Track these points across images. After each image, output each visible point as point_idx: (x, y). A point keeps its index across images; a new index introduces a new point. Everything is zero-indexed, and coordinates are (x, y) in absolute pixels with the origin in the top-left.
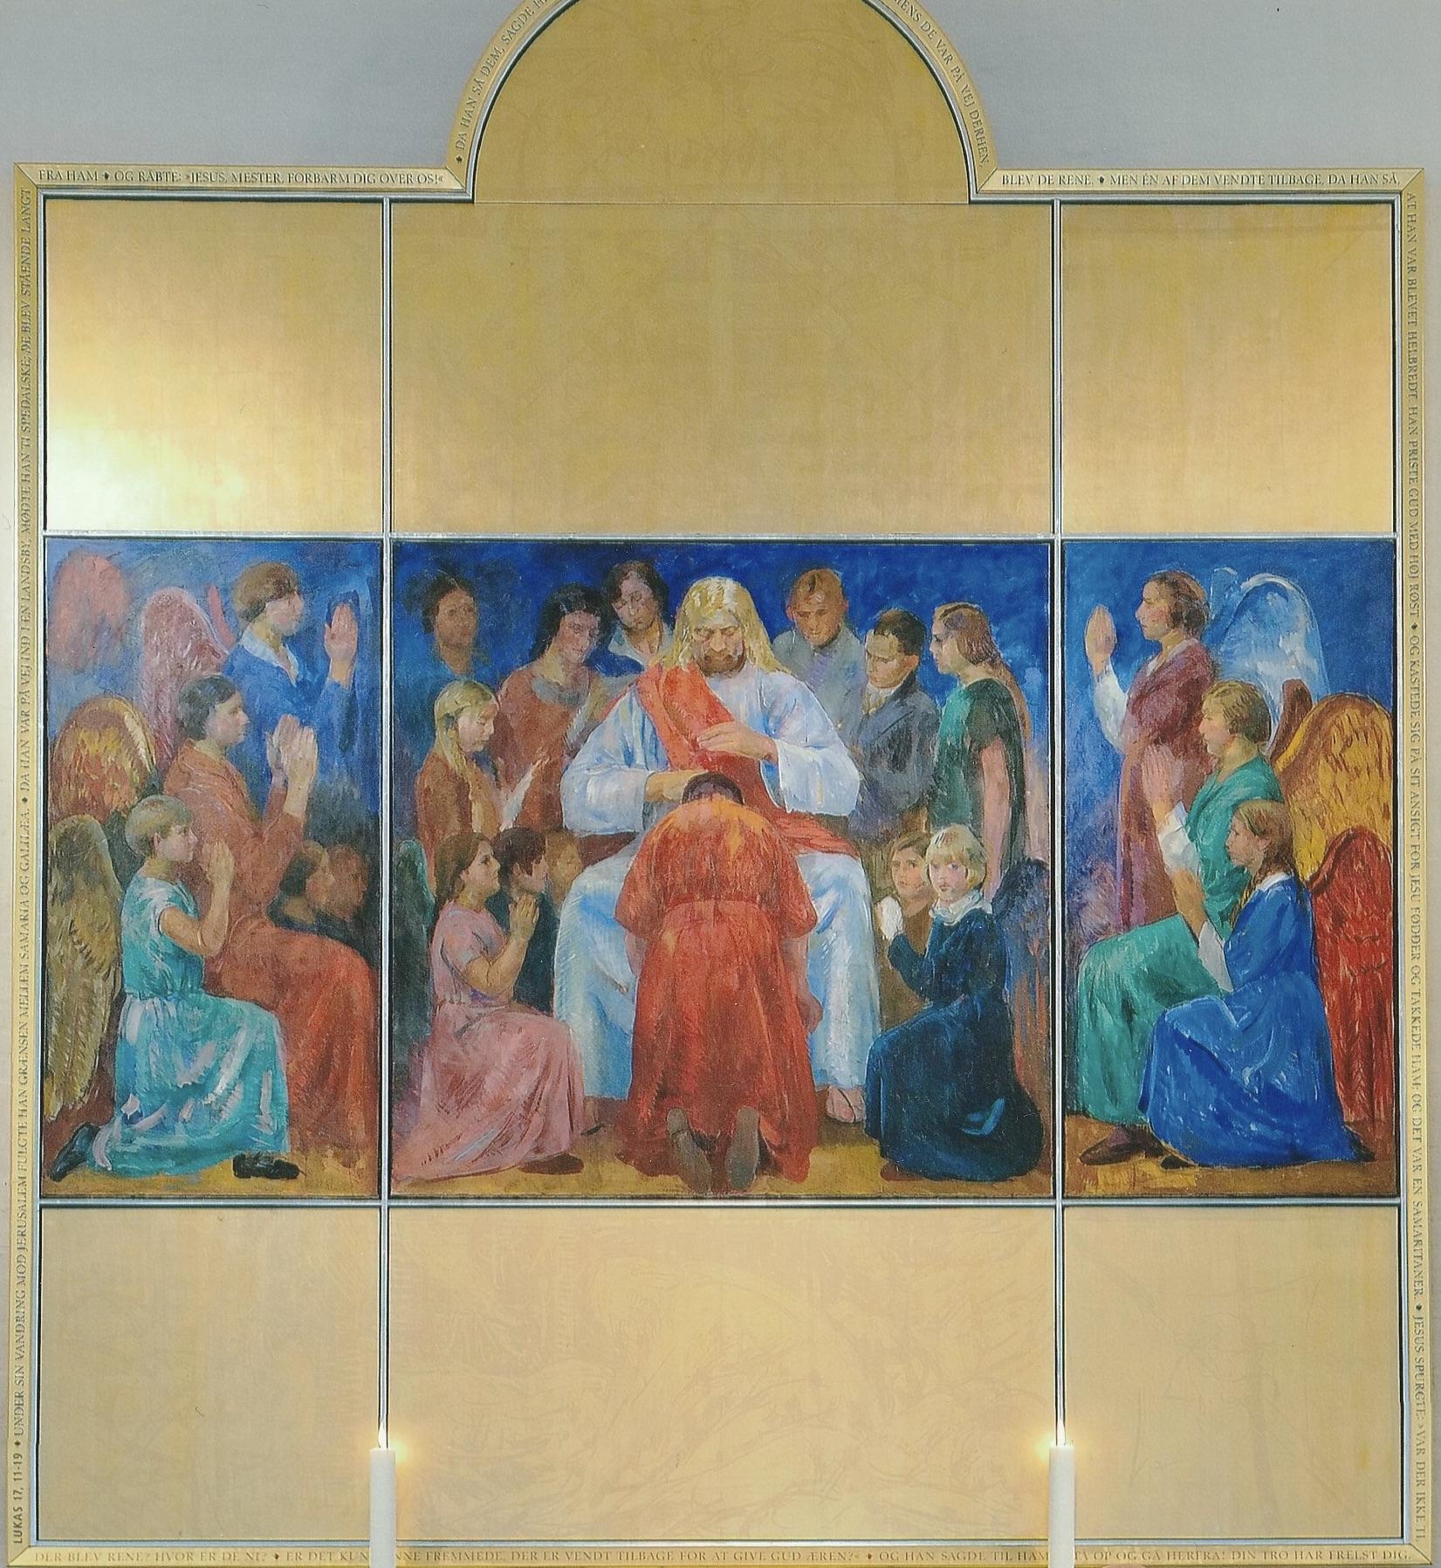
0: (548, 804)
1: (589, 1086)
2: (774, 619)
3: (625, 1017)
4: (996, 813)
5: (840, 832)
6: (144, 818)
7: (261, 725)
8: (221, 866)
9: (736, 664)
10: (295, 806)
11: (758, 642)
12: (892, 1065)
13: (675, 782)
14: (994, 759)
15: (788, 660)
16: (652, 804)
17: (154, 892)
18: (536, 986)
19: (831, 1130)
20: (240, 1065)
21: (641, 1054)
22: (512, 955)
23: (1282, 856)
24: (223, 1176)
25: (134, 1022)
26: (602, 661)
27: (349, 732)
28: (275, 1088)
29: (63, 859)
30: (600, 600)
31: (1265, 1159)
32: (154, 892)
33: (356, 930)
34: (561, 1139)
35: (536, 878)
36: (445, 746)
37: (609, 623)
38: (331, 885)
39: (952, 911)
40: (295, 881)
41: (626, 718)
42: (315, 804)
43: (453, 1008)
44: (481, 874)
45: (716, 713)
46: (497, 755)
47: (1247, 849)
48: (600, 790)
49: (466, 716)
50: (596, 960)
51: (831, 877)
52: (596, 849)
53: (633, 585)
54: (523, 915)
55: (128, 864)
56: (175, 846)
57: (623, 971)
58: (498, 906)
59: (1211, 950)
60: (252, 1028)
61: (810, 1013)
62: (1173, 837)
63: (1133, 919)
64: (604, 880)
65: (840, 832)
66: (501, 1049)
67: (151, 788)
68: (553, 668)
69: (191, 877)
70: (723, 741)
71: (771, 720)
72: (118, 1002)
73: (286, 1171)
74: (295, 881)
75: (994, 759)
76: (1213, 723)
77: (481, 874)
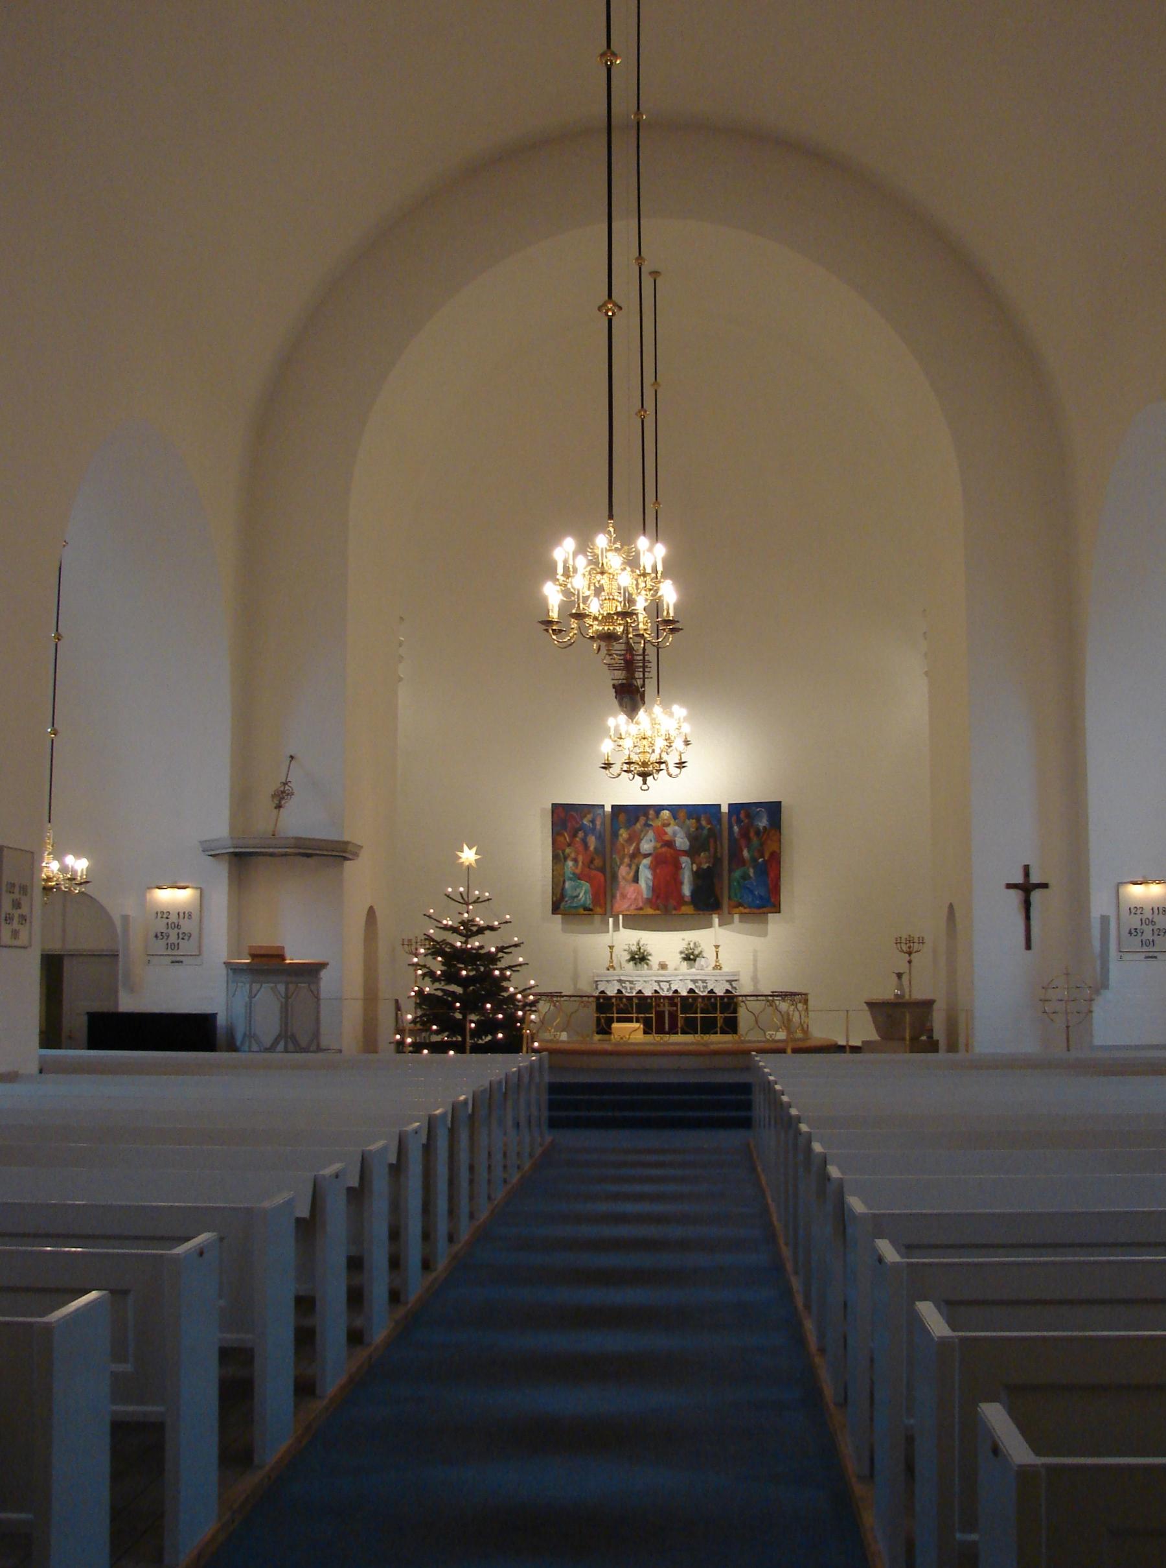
0: (638, 849)
1: (645, 896)
2: (675, 818)
3: (651, 884)
4: (712, 850)
5: (686, 853)
6: (568, 850)
7: (586, 835)
8: (580, 858)
9: (669, 825)
10: (592, 848)
11: (672, 822)
12: (694, 893)
13: (659, 845)
14: (712, 840)
15: (677, 825)
16: (655, 848)
17: (570, 863)
18: (636, 879)
19: (685, 903)
20: (583, 893)
21: (654, 890)
22: (632, 874)
23: (762, 856)
24: (582, 911)
25: (567, 885)
26: (647, 825)
27: (600, 838)
28: (589, 896)
29: (555, 857)
30: (646, 815)
31: (759, 907)
32: (570, 863)
33: (602, 870)
34: (641, 904)
35: (636, 861)
36: (621, 839)
37: (648, 818)
38: (598, 862)
39: (705, 866)
40: (592, 862)
41: (651, 834)
42: (595, 848)
43: (622, 883)
44: (627, 860)
45: (666, 833)
46: (630, 840)
47: (756, 854)
48: (646, 846)
49: (624, 834)
50: (646, 875)
51: (685, 861)
52: (646, 856)
53: (651, 812)
54: (634, 867)
55: (565, 859)
56: (573, 855)
57: (650, 876)
58: (630, 866)
59: (751, 872)
60: (586, 886)
61: (682, 883)
62: (746, 853)
63: (336, 1047)
64: (646, 861)
65: (686, 853)
66: (630, 890)
67: (569, 845)
68: (638, 826)
69: (575, 860)
70: (666, 838)
71: (675, 834)
72: (564, 882)
73: (590, 910)
74: (592, 862)
75: (712, 840)
76: (752, 834)
77: (627, 860)
